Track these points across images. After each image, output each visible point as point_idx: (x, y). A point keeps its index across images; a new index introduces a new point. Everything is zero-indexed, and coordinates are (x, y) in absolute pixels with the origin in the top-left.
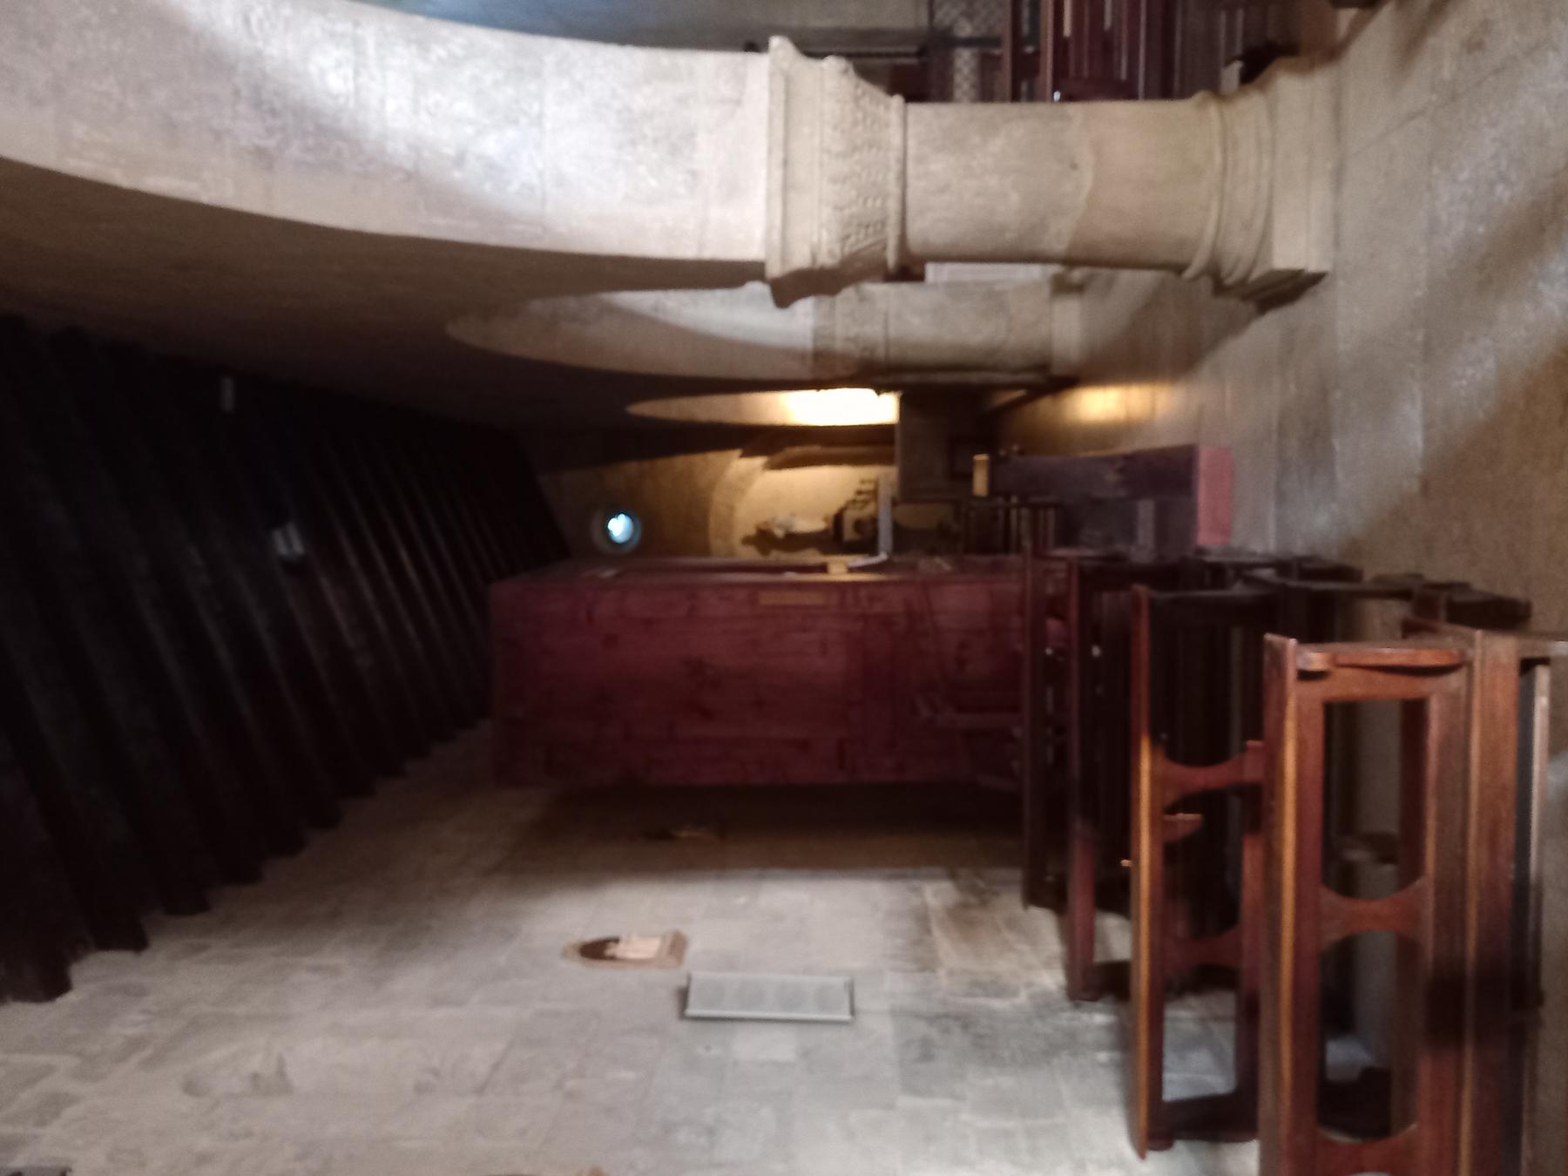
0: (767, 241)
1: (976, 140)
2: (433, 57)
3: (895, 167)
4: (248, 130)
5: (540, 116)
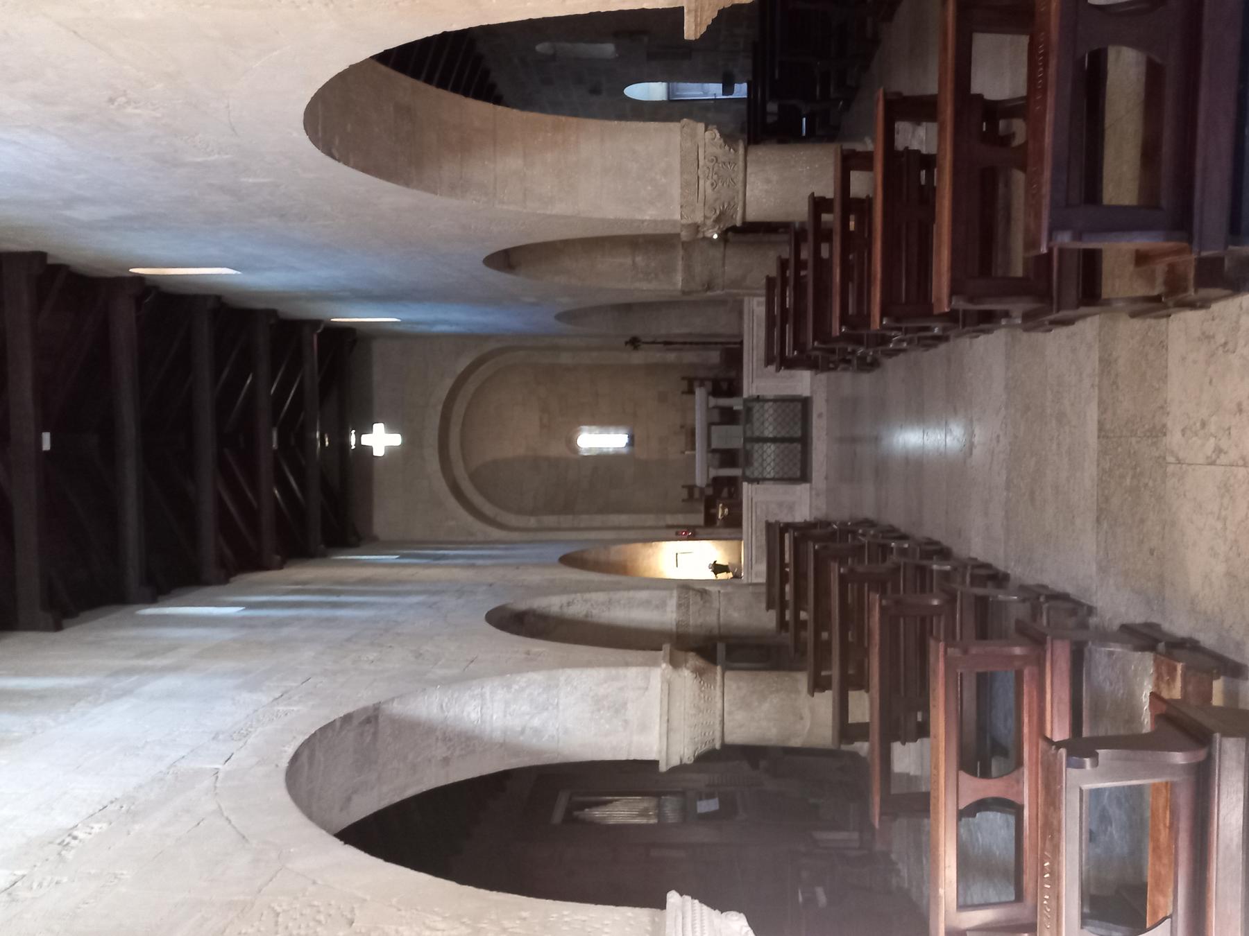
0: (660, 752)
1: (756, 704)
2: (513, 690)
3: (718, 719)
4: (440, 751)
5: (558, 704)
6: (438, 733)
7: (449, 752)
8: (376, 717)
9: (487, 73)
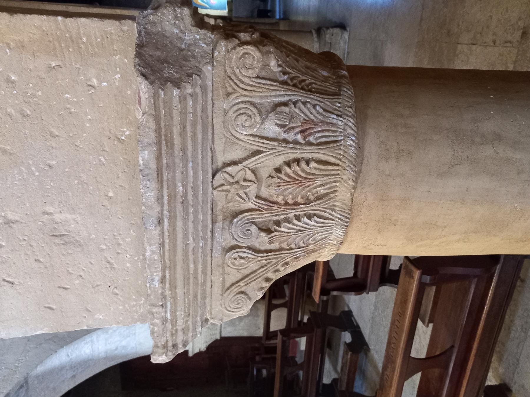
2: (109, 333)
4: (70, 374)
6: (68, 368)
7: (17, 283)
8: (27, 382)
9: (254, 152)
